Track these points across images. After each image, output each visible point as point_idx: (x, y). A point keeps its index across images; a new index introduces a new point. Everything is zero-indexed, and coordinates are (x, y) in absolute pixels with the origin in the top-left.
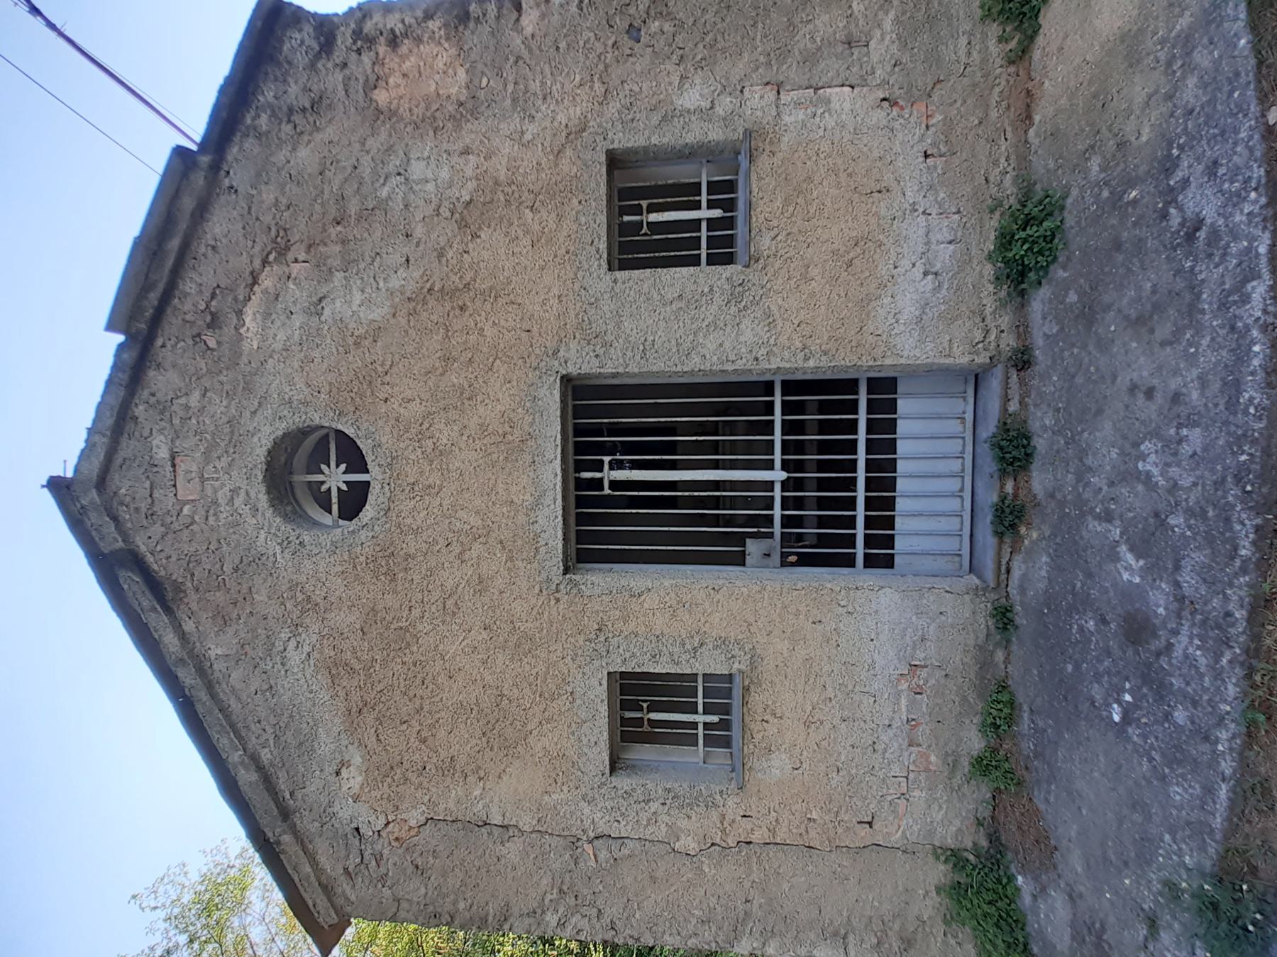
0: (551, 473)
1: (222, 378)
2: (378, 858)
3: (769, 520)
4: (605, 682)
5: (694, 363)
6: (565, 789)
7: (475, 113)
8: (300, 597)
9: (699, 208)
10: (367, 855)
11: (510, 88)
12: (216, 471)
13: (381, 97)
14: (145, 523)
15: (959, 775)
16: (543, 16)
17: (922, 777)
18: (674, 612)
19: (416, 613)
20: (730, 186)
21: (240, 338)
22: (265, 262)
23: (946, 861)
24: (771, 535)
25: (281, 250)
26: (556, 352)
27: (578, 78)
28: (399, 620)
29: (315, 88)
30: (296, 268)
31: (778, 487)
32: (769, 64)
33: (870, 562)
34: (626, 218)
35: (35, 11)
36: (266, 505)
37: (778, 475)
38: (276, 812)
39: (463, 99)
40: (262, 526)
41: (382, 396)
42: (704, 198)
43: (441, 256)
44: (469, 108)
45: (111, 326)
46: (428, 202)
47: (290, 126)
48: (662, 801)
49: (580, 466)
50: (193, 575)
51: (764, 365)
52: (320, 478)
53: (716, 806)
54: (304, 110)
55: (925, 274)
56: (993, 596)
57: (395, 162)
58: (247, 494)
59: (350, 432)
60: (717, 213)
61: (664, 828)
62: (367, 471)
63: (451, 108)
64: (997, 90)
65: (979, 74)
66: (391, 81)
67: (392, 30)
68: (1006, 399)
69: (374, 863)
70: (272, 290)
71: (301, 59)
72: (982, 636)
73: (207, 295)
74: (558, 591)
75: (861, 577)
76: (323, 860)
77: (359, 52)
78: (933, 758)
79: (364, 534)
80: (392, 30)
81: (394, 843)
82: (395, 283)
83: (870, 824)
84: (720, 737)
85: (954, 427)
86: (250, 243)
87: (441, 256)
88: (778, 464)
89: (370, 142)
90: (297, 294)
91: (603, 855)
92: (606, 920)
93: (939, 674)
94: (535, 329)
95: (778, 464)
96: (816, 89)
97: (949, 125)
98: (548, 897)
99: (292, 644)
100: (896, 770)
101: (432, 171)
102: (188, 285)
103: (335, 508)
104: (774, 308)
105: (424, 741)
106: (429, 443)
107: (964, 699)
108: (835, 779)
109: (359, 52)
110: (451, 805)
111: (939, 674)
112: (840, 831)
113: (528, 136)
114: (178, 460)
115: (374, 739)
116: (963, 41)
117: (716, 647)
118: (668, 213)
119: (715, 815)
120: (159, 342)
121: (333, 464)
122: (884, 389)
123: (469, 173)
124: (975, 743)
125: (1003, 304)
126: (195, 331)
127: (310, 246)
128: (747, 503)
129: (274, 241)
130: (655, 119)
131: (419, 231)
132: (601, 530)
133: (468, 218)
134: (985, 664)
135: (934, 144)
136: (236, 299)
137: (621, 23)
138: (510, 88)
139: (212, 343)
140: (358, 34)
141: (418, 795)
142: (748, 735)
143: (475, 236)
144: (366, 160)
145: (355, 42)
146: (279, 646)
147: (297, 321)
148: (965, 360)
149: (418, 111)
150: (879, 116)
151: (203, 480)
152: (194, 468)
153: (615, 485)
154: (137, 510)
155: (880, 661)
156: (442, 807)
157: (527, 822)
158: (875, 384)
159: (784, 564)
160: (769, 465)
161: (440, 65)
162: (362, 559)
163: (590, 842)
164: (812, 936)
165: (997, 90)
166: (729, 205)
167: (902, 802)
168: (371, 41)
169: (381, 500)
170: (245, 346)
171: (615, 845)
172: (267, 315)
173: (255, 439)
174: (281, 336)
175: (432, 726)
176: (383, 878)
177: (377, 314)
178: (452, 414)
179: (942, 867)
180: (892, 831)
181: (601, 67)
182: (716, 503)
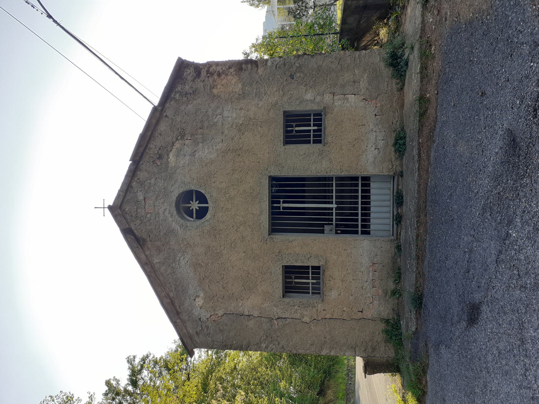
2: (207, 327)
3: (332, 220)
4: (281, 269)
7: (244, 98)
9: (310, 126)
10: (203, 327)
11: (255, 91)
13: (215, 91)
16: (265, 69)
17: (377, 296)
18: (302, 247)
19: (222, 248)
21: (168, 162)
22: (177, 139)
24: (332, 224)
25: (182, 136)
26: (267, 169)
27: (275, 89)
28: (217, 250)
29: (194, 87)
30: (187, 142)
31: (334, 209)
32: (331, 87)
34: (289, 129)
35: (50, 16)
36: (176, 214)
37: (334, 206)
38: (175, 312)
39: (240, 93)
42: (312, 123)
43: (232, 139)
44: (243, 96)
45: (130, 161)
46: (229, 123)
49: (273, 202)
50: (150, 236)
52: (190, 205)
53: (315, 307)
54: (190, 94)
55: (375, 149)
56: (396, 242)
57: (219, 111)
58: (169, 210)
59: (203, 192)
60: (316, 128)
61: (299, 315)
62: (208, 203)
63: (237, 96)
64: (395, 98)
65: (390, 93)
66: (218, 86)
67: (219, 71)
68: (398, 185)
69: (206, 329)
70: (179, 148)
71: (190, 78)
73: (158, 149)
75: (360, 237)
76: (189, 329)
77: (208, 77)
78: (380, 291)
80: (219, 71)
82: (218, 147)
83: (362, 312)
84: (317, 291)
85: (387, 191)
86: (172, 133)
87: (232, 139)
88: (334, 202)
90: (187, 150)
91: (280, 324)
92: (281, 345)
93: (381, 265)
94: (261, 162)
95: (334, 202)
97: (382, 106)
100: (369, 295)
101: (230, 114)
102: (151, 146)
103: (194, 215)
105: (224, 288)
107: (388, 273)
108: (351, 298)
109: (208, 77)
110: (232, 309)
111: (381, 265)
113: (260, 106)
114: (146, 200)
115: (208, 288)
116: (386, 84)
117: (315, 258)
118: (302, 127)
119: (315, 310)
120: (141, 163)
121: (194, 201)
122: (366, 180)
123: (242, 115)
124: (392, 286)
125: (397, 159)
127: (192, 135)
130: (298, 102)
131: (226, 132)
132: (280, 222)
133: (241, 128)
134: (394, 262)
135: (377, 112)
136: (167, 150)
137: (288, 74)
138: (255, 91)
139: (159, 164)
140: (208, 72)
142: (324, 285)
143: (243, 134)
144: (210, 110)
145: (207, 74)
147: (187, 158)
150: (362, 104)
151: (154, 206)
152: (152, 202)
153: (284, 208)
154: (132, 216)
155: (364, 262)
156: (229, 309)
157: (256, 314)
159: (336, 233)
161: (233, 82)
162: (206, 231)
163: (276, 320)
164: (345, 348)
165: (395, 98)
167: (371, 305)
168: (212, 74)
170: (170, 165)
171: (283, 320)
172: (178, 156)
173: (173, 194)
174: (182, 162)
175: (226, 283)
176: (208, 334)
177: (213, 156)
178: (235, 187)
179: (383, 325)
180: (369, 314)
181: (282, 86)
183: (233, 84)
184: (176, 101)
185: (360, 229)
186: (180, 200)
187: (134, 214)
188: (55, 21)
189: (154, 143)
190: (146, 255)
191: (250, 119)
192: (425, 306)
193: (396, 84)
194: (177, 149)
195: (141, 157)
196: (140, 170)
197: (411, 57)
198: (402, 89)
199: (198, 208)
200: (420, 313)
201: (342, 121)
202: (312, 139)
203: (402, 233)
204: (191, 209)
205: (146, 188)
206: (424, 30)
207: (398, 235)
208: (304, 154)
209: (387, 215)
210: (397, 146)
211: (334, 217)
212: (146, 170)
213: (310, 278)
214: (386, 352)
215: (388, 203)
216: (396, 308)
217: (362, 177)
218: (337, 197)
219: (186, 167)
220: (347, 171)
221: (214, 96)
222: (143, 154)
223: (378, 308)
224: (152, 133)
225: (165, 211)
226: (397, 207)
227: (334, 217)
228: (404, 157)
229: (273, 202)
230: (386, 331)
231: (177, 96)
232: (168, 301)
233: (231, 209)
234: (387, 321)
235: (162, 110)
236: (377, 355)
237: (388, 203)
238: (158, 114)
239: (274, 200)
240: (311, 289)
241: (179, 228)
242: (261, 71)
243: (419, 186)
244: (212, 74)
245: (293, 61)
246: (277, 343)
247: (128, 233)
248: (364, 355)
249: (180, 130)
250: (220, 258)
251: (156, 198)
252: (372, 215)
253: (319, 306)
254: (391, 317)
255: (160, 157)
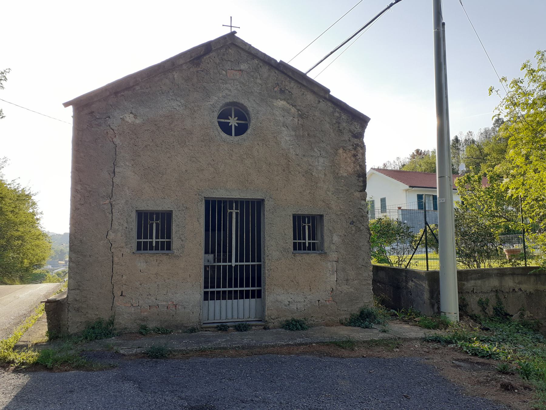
0: (236, 195)
1: (265, 91)
2: (99, 125)
3: (219, 261)
4: (169, 209)
5: (267, 238)
6: (130, 194)
8: (196, 109)
11: (341, 188)
12: (237, 85)
13: (341, 151)
14: (219, 57)
15: (140, 322)
16: (358, 198)
18: (190, 231)
20: (314, 249)
21: (277, 99)
22: (298, 110)
23: (109, 320)
24: (215, 262)
25: (301, 116)
29: (344, 131)
30: (296, 120)
31: (230, 264)
32: (343, 259)
33: (206, 293)
34: (307, 219)
40: (218, 99)
41: (259, 143)
42: (311, 241)
44: (337, 177)
47: (335, 122)
48: (128, 227)
51: (266, 258)
52: (233, 116)
53: (126, 245)
54: (339, 127)
55: (289, 302)
56: (199, 327)
57: (324, 153)
58: (230, 95)
59: (249, 131)
60: (307, 245)
61: (117, 228)
66: (345, 154)
71: (353, 127)
72: (186, 325)
74: (199, 195)
77: (353, 145)
78: (146, 313)
79: (217, 133)
81: (105, 131)
82: (291, 151)
83: (122, 295)
85: (247, 315)
88: (237, 264)
89: (329, 146)
93: (174, 313)
95: (237, 264)
96: (336, 271)
98: (87, 187)
99: (180, 104)
100: (141, 302)
101: (321, 164)
102: (293, 84)
104: (281, 261)
105: (146, 146)
106: (245, 157)
107: (166, 321)
108: (138, 283)
111: (174, 313)
112: (119, 286)
113: (328, 193)
116: (346, 309)
117: (181, 245)
118: (307, 231)
119: (124, 245)
122: (258, 295)
126: (280, 84)
128: (225, 255)
129: (304, 114)
130: (331, 228)
131: (305, 159)
133: (308, 173)
134: (177, 327)
136: (288, 99)
138: (341, 188)
139: (276, 89)
141: (126, 143)
146: (178, 99)
147: (281, 119)
148: (266, 314)
149: (336, 161)
150: (329, 288)
151: (234, 80)
154: (224, 55)
157: (117, 180)
158: (259, 292)
160: (236, 261)
161: (348, 168)
162: (209, 131)
166: (309, 249)
168: (355, 149)
169: (228, 140)
170: (274, 101)
172: (283, 109)
173: (247, 100)
174: (277, 113)
180: (119, 303)
182: (225, 252)
183: (347, 168)
184: (333, 113)
185: (210, 290)
186: (238, 106)
187: (225, 57)
188: (392, 5)
189: (295, 87)
190: (182, 65)
191: (317, 183)
192: (156, 362)
193: (346, 318)
194: (290, 109)
195: (283, 72)
196: (269, 70)
197: (376, 331)
198: (342, 324)
199: (230, 125)
200: (144, 357)
201: (314, 270)
202: (297, 241)
203: (209, 332)
204: (230, 117)
205: (252, 74)
206: (405, 341)
207: (206, 329)
208: (285, 234)
209: (224, 316)
210: (294, 322)
211: (222, 264)
212: (269, 75)
213: (157, 240)
214: (74, 323)
215: (236, 317)
216: (126, 332)
217: (261, 290)
218: (241, 266)
219: (271, 115)
220: (269, 275)
221: (337, 150)
222: (285, 74)
223: (126, 313)
224: (304, 86)
225: (228, 92)
226: (235, 326)
227: (222, 264)
228: (283, 330)
229: (236, 202)
230: (100, 323)
231: (337, 114)
232: (131, 84)
233: (232, 159)
234: (112, 323)
235: (325, 98)
236: (70, 314)
237: (241, 316)
238: (322, 94)
239: (241, 204)
240: (145, 240)
241: (211, 103)
242: (357, 194)
243: (273, 346)
244: (355, 149)
245: (365, 224)
246: (82, 203)
247: (207, 49)
248: (70, 300)
249: (306, 114)
250: (180, 144)
251: (243, 83)
252: (224, 302)
253: (127, 250)
254: (116, 327)
255: (282, 91)
